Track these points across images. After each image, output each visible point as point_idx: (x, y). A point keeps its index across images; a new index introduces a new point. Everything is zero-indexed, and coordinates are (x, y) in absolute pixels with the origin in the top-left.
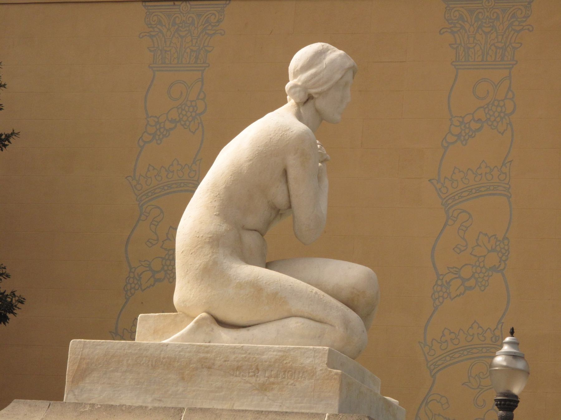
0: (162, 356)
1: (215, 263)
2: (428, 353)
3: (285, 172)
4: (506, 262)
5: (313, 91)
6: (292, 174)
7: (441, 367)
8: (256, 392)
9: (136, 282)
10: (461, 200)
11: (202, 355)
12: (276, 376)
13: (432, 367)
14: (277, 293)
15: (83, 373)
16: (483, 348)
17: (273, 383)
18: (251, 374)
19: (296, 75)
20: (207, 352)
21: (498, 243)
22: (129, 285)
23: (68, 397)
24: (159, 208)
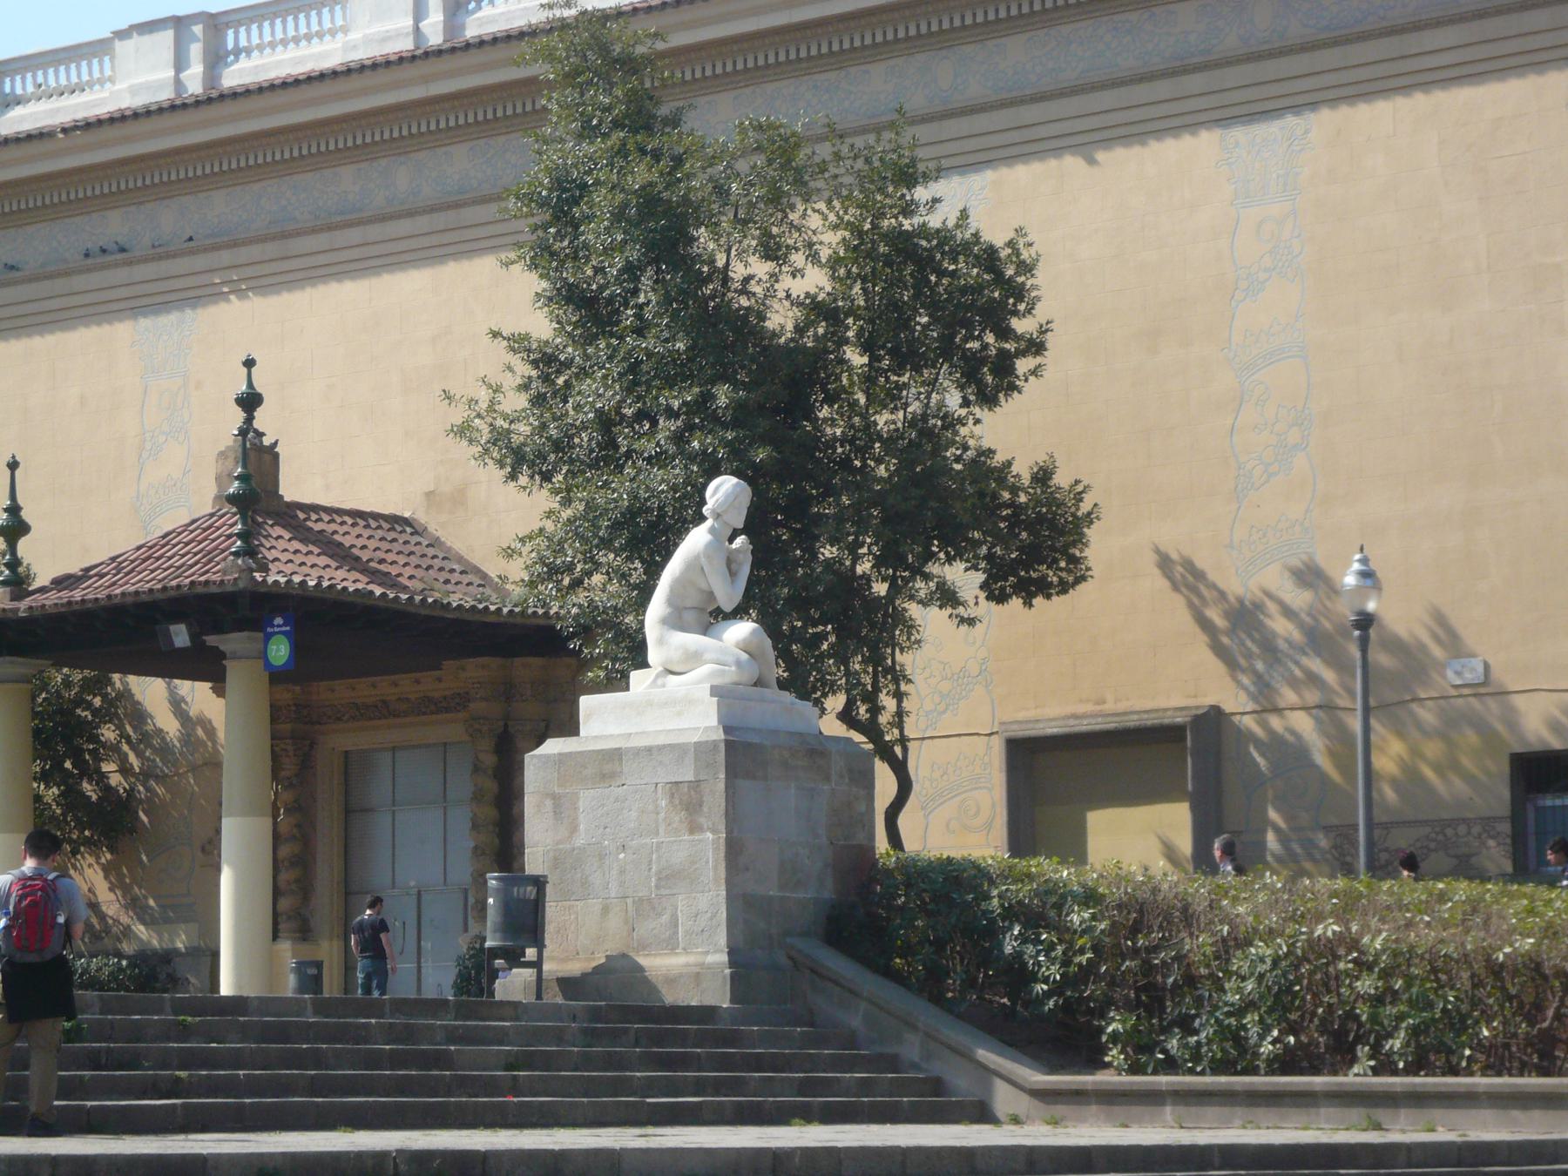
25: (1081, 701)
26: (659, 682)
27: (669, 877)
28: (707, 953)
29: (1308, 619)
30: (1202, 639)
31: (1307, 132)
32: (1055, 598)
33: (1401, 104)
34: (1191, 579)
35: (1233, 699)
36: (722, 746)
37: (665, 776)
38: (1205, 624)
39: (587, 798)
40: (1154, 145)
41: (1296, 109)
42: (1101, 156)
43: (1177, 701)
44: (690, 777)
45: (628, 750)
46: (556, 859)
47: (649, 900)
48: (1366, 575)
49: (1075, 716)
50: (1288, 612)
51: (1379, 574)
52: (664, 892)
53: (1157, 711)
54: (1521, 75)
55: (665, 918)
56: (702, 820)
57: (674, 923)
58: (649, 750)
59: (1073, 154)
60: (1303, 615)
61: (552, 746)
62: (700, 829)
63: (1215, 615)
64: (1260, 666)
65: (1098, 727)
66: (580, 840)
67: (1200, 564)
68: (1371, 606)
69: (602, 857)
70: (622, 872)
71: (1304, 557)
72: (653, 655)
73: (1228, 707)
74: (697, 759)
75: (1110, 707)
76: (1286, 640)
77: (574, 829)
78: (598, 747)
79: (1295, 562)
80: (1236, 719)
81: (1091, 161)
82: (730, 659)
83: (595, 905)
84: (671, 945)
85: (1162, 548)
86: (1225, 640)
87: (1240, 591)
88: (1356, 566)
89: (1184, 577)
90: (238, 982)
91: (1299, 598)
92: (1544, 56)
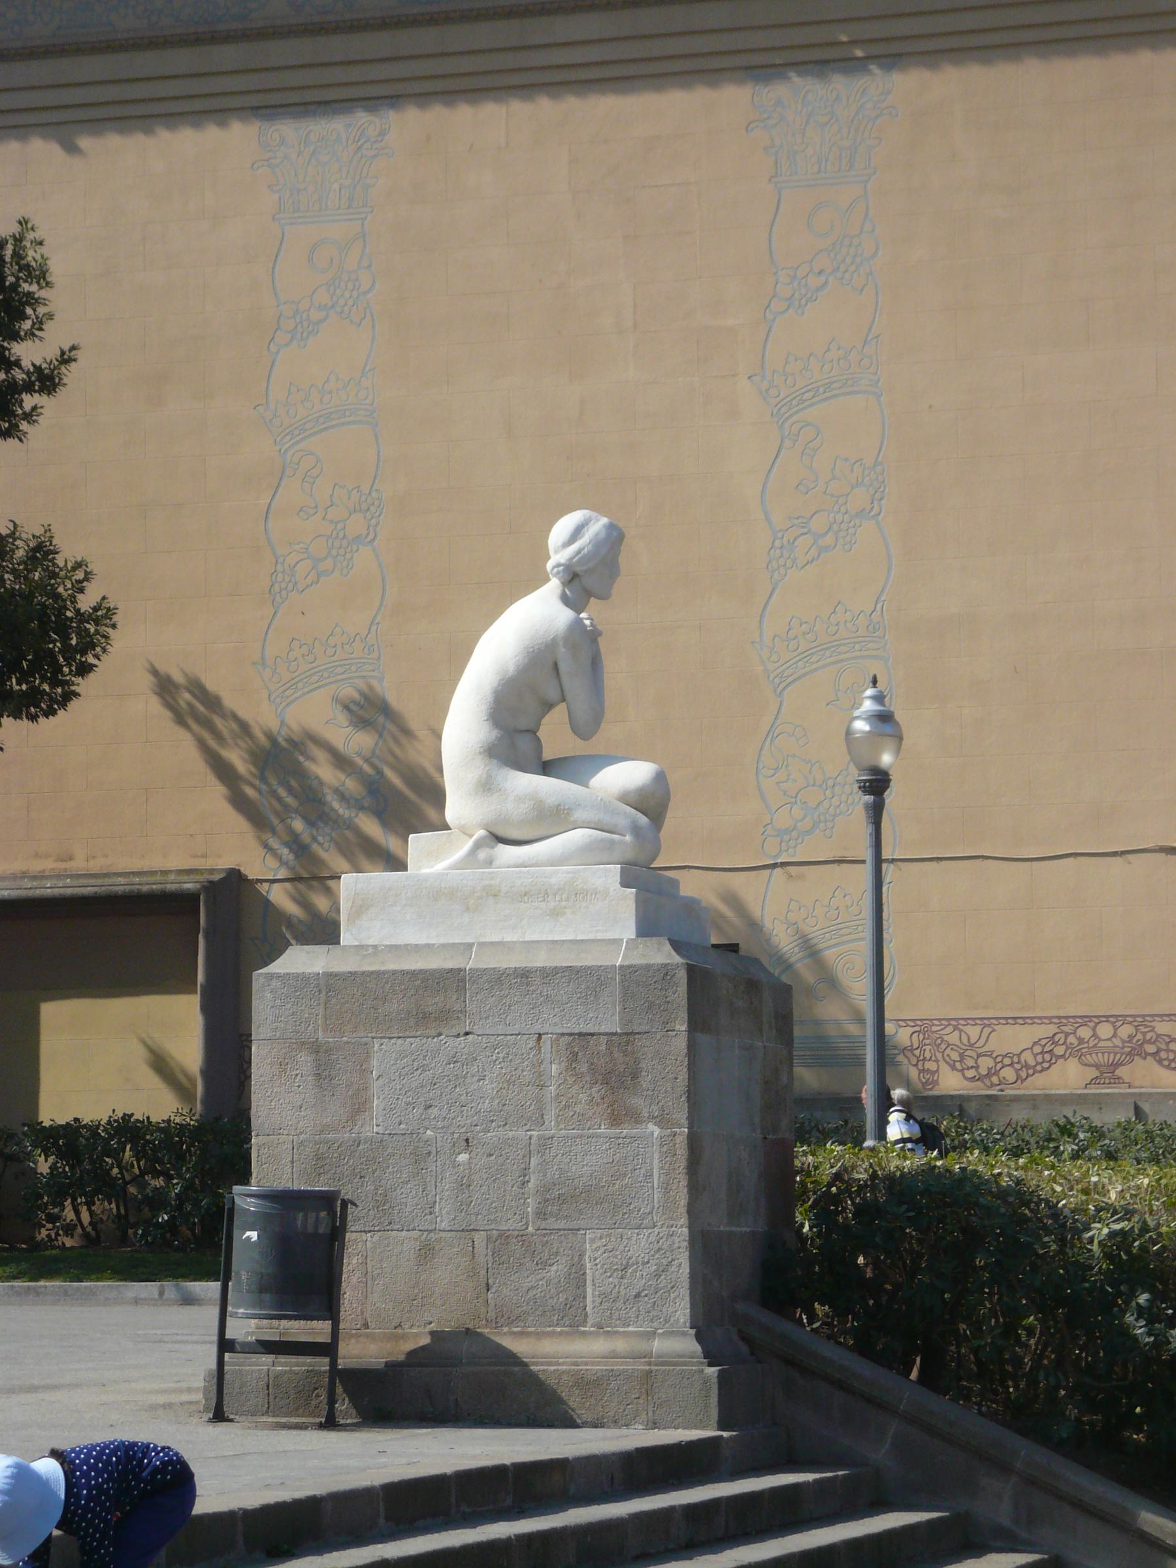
1: (489, 777)
3: (556, 666)
4: (883, 502)
5: (578, 569)
6: (563, 668)
7: (790, 679)
9: (287, 579)
10: (801, 406)
11: (487, 883)
12: (567, 900)
13: (777, 681)
15: (360, 910)
19: (556, 552)
20: (492, 879)
21: (866, 472)
22: (276, 585)
23: (346, 938)
24: (312, 454)
25: (37, 855)
26: (482, 855)
27: (564, 1201)
28: (652, 1335)
29: (366, 768)
30: (218, 790)
31: (382, 134)
32: (42, 720)
33: (519, 108)
34: (201, 708)
35: (257, 861)
36: (682, 975)
37: (554, 1023)
38: (223, 771)
39: (387, 1056)
40: (164, 134)
41: (372, 103)
42: (85, 142)
43: (176, 862)
44: (613, 1024)
45: (477, 974)
47: (522, 1237)
48: (884, 718)
49: (24, 875)
50: (341, 761)
51: (897, 717)
52: (551, 1223)
53: (153, 873)
54: (687, 86)
56: (637, 1102)
57: (577, 1279)
59: (44, 137)
60: (359, 761)
61: (300, 960)
62: (636, 1118)
63: (237, 758)
64: (298, 825)
65: (69, 892)
66: (373, 1126)
67: (212, 685)
68: (886, 759)
69: (419, 1158)
70: (464, 1185)
71: (361, 684)
72: (456, 807)
73: (251, 873)
74: (626, 994)
75: (78, 864)
76: (337, 791)
77: (359, 1107)
78: (392, 966)
79: (348, 692)
80: (264, 888)
81: (71, 148)
82: (622, 822)
83: (405, 1243)
84: (571, 1317)
85: (162, 668)
86: (250, 792)
87: (273, 725)
88: (868, 706)
89: (190, 704)
91: (355, 742)
92: (716, 63)
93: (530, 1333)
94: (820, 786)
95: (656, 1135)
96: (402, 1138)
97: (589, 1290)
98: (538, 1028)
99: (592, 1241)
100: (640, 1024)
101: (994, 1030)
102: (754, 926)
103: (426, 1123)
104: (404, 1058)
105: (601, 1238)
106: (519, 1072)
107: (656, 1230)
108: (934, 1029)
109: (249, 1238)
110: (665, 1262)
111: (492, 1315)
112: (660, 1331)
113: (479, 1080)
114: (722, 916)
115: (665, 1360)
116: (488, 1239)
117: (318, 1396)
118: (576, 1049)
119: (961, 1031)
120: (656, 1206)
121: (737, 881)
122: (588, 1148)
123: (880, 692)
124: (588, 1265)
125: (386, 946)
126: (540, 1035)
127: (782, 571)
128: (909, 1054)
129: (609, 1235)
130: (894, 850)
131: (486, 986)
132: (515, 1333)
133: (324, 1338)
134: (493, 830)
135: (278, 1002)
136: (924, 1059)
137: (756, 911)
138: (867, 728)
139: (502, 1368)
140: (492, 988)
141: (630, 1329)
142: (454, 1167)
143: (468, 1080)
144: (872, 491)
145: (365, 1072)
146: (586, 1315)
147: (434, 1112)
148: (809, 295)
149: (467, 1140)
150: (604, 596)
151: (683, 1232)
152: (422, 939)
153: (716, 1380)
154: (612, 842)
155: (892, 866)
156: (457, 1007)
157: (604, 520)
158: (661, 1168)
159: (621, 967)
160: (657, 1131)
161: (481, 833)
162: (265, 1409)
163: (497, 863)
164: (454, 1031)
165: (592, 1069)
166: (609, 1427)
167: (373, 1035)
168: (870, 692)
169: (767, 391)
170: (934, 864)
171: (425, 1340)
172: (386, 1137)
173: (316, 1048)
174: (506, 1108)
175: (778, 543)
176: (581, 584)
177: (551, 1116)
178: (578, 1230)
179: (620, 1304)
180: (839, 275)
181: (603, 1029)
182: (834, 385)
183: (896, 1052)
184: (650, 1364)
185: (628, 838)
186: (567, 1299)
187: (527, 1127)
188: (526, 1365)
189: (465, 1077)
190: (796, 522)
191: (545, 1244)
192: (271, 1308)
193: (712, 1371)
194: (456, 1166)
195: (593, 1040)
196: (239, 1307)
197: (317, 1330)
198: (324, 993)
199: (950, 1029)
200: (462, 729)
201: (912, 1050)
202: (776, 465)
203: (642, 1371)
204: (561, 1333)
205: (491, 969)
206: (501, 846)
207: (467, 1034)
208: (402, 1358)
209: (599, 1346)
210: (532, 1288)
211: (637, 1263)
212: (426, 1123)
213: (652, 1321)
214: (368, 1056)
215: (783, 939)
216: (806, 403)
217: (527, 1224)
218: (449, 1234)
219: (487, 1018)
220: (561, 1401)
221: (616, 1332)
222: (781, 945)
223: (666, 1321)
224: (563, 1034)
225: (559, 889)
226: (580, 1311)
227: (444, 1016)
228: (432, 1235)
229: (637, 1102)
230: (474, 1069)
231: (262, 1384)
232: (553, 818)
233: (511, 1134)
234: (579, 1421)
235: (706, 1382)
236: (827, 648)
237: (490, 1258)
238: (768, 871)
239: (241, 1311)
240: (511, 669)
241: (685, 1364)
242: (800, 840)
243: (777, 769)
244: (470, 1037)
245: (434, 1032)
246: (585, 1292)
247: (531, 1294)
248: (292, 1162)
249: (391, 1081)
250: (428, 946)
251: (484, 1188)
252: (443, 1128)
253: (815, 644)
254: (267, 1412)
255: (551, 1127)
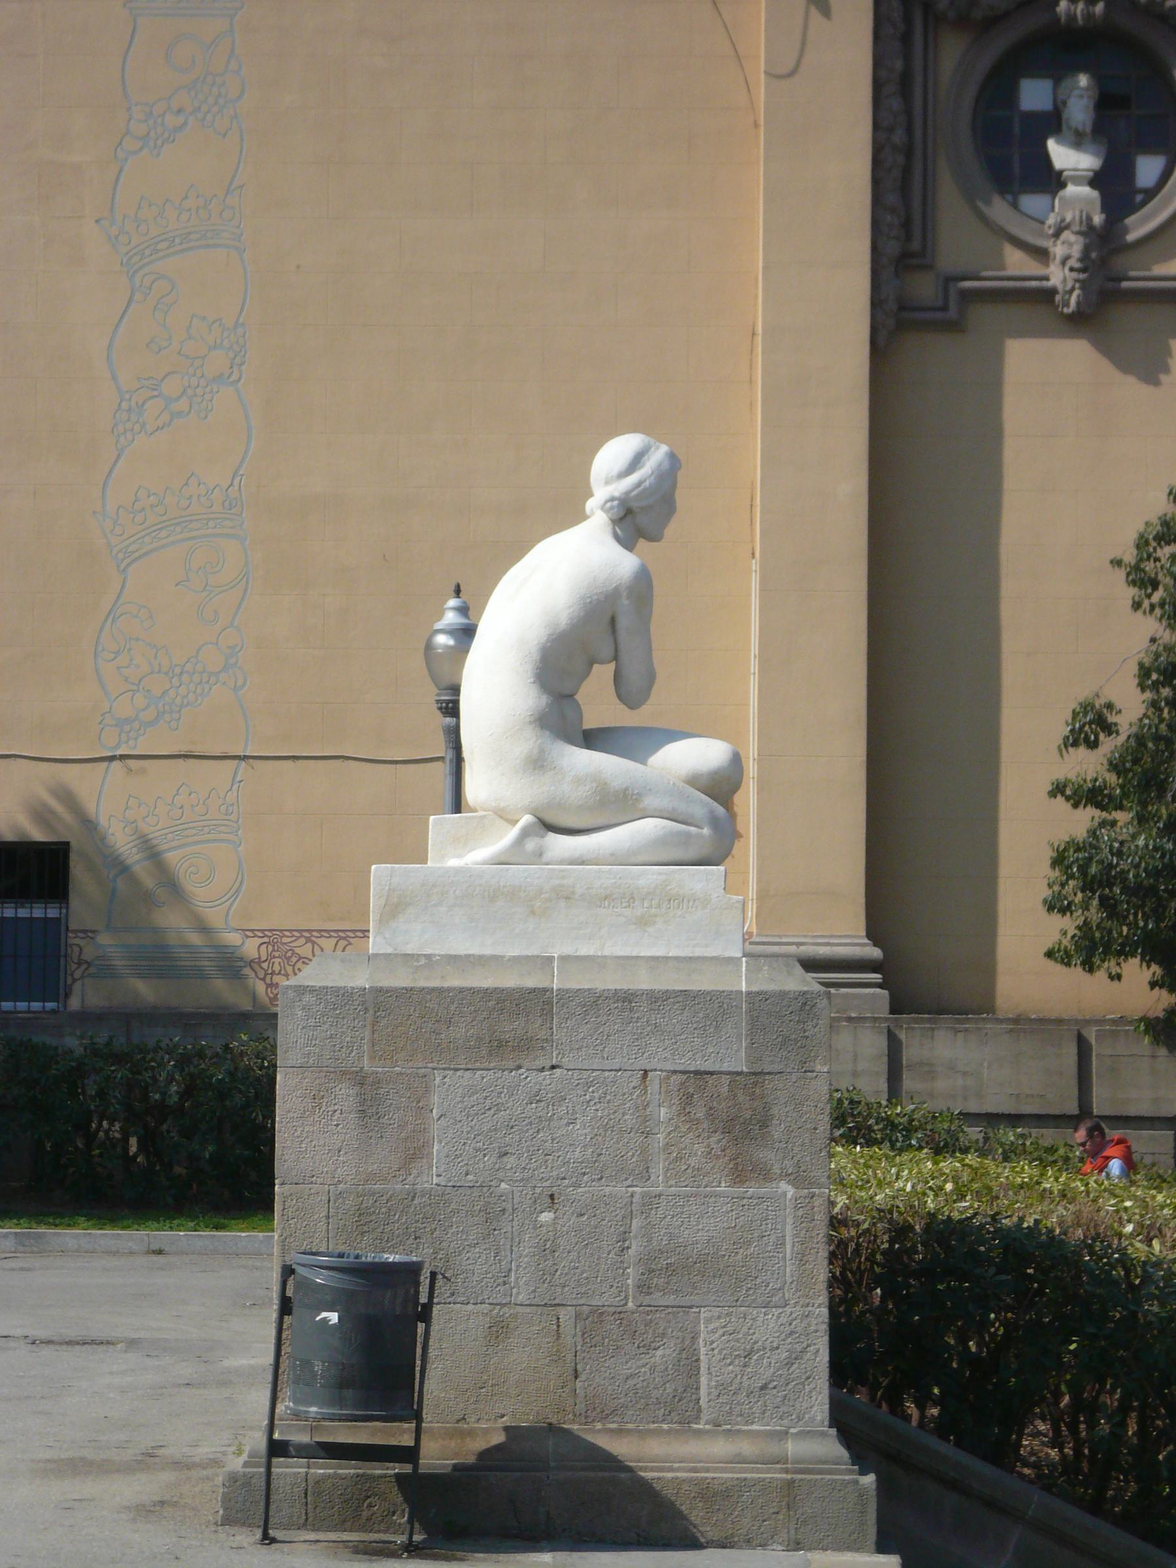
0: (502, 884)
1: (542, 751)
2: (112, 531)
3: (613, 621)
4: (243, 367)
5: (635, 505)
7: (136, 555)
8: (633, 927)
11: (557, 882)
13: (121, 556)
14: (627, 789)
15: (395, 908)
16: (209, 519)
17: (656, 916)
18: (624, 904)
20: (563, 877)
21: (225, 335)
26: (531, 845)
27: (674, 1271)
28: (784, 1435)
37: (663, 1057)
39: (450, 1092)
46: (361, 1212)
47: (620, 1314)
52: (657, 1298)
55: (663, 1354)
56: (767, 1155)
57: (689, 1366)
58: (627, 998)
62: (766, 1175)
66: (433, 1175)
69: (492, 1215)
70: (547, 1249)
77: (415, 1153)
78: (455, 982)
84: (681, 1411)
88: (451, 618)
90: (279, 1475)
93: (629, 1431)
94: (167, 673)
95: (789, 1195)
96: (469, 1192)
97: (704, 1380)
98: (643, 1063)
99: (708, 1321)
100: (772, 1062)
101: (350, 944)
102: (89, 824)
103: (501, 1174)
104: (473, 1094)
105: (719, 1317)
106: (618, 1115)
107: (788, 1310)
108: (285, 940)
109: (325, 1320)
110: (799, 1348)
111: (581, 1407)
112: (792, 1431)
113: (568, 1124)
114: (52, 812)
115: (804, 1467)
116: (577, 1316)
117: (370, 1506)
118: (691, 1090)
119: (314, 943)
120: (789, 1280)
121: (70, 775)
122: (703, 1208)
123: (464, 602)
124: (703, 1350)
125: (442, 956)
126: (646, 1071)
127: (129, 435)
128: (256, 967)
129: (729, 1314)
130: (246, 746)
131: (579, 1010)
132: (612, 1430)
133: (408, 1441)
134: (541, 815)
135: (312, 1022)
136: (273, 973)
137: (91, 808)
138: (451, 642)
139: (606, 1474)
140: (586, 1013)
141: (755, 1427)
142: (535, 1228)
143: (554, 1124)
144: (231, 354)
145: (422, 1110)
146: (700, 1410)
147: (510, 1161)
148: (166, 135)
149: (552, 1196)
150: (654, 537)
151: (821, 1313)
152: (475, 950)
153: (874, 1493)
154: (688, 835)
155: (243, 764)
156: (542, 1035)
157: (664, 449)
158: (796, 1236)
159: (749, 993)
160: (791, 1192)
161: (527, 819)
162: (302, 1521)
163: (548, 856)
164: (539, 1063)
165: (711, 1114)
166: (741, 1548)
167: (435, 1065)
168: (453, 602)
169: (116, 237)
170: (290, 763)
171: (499, 1438)
172: (448, 1190)
173: (360, 1079)
174: (602, 1158)
175: (124, 405)
176: (635, 521)
177: (659, 1169)
178: (691, 1307)
179: (742, 1397)
180: (200, 115)
181: (725, 1067)
182: (192, 236)
183: (242, 964)
184: (787, 1471)
185: (706, 831)
186: (675, 1390)
187: (629, 1182)
188: (630, 1470)
189: (550, 1119)
190: (146, 383)
191: (648, 1324)
192: (355, 1408)
193: (869, 1480)
194: (537, 1226)
195: (711, 1080)
196: (311, 1405)
197: (400, 1435)
198: (371, 1012)
199: (303, 940)
200: (495, 686)
201: (260, 962)
202: (125, 320)
203: (782, 1480)
204: (669, 1432)
205: (585, 990)
206: (551, 835)
207: (553, 1067)
208: (471, 1460)
209: (720, 1448)
210: (632, 1376)
211: (765, 1348)
212: (501, 1174)
213: (781, 1418)
214: (427, 1090)
215: (121, 840)
216: (161, 254)
217: (626, 1298)
218: (528, 1310)
219: (580, 1049)
220: (684, 1517)
221: (739, 1431)
222: (117, 846)
223: (799, 1419)
224: (675, 1072)
225: (649, 894)
226: (691, 1405)
227: (526, 1045)
228: (506, 1309)
229: (767, 1155)
230: (562, 1110)
231: (298, 1490)
232: (619, 805)
233: (607, 1190)
234: (703, 1540)
235: (862, 1494)
236: (178, 524)
237: (579, 1339)
238: (105, 764)
239: (314, 1409)
240: (564, 621)
241: (830, 1472)
242: (141, 732)
243: (118, 653)
244: (558, 1071)
245: (511, 1065)
246: (698, 1382)
247: (631, 1382)
248: (328, 1217)
249: (456, 1122)
250: (496, 958)
251: (574, 1255)
252: (522, 1180)
253: (164, 518)
254: (305, 1525)
255: (659, 1181)
